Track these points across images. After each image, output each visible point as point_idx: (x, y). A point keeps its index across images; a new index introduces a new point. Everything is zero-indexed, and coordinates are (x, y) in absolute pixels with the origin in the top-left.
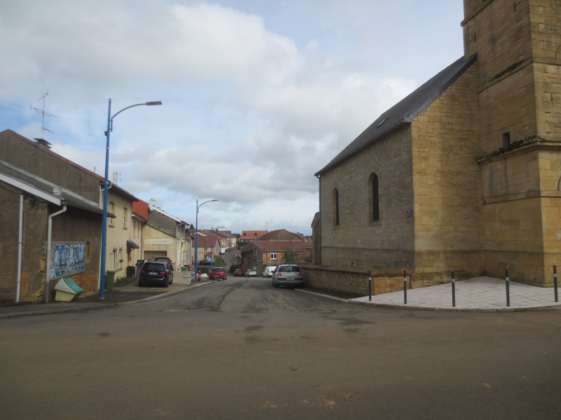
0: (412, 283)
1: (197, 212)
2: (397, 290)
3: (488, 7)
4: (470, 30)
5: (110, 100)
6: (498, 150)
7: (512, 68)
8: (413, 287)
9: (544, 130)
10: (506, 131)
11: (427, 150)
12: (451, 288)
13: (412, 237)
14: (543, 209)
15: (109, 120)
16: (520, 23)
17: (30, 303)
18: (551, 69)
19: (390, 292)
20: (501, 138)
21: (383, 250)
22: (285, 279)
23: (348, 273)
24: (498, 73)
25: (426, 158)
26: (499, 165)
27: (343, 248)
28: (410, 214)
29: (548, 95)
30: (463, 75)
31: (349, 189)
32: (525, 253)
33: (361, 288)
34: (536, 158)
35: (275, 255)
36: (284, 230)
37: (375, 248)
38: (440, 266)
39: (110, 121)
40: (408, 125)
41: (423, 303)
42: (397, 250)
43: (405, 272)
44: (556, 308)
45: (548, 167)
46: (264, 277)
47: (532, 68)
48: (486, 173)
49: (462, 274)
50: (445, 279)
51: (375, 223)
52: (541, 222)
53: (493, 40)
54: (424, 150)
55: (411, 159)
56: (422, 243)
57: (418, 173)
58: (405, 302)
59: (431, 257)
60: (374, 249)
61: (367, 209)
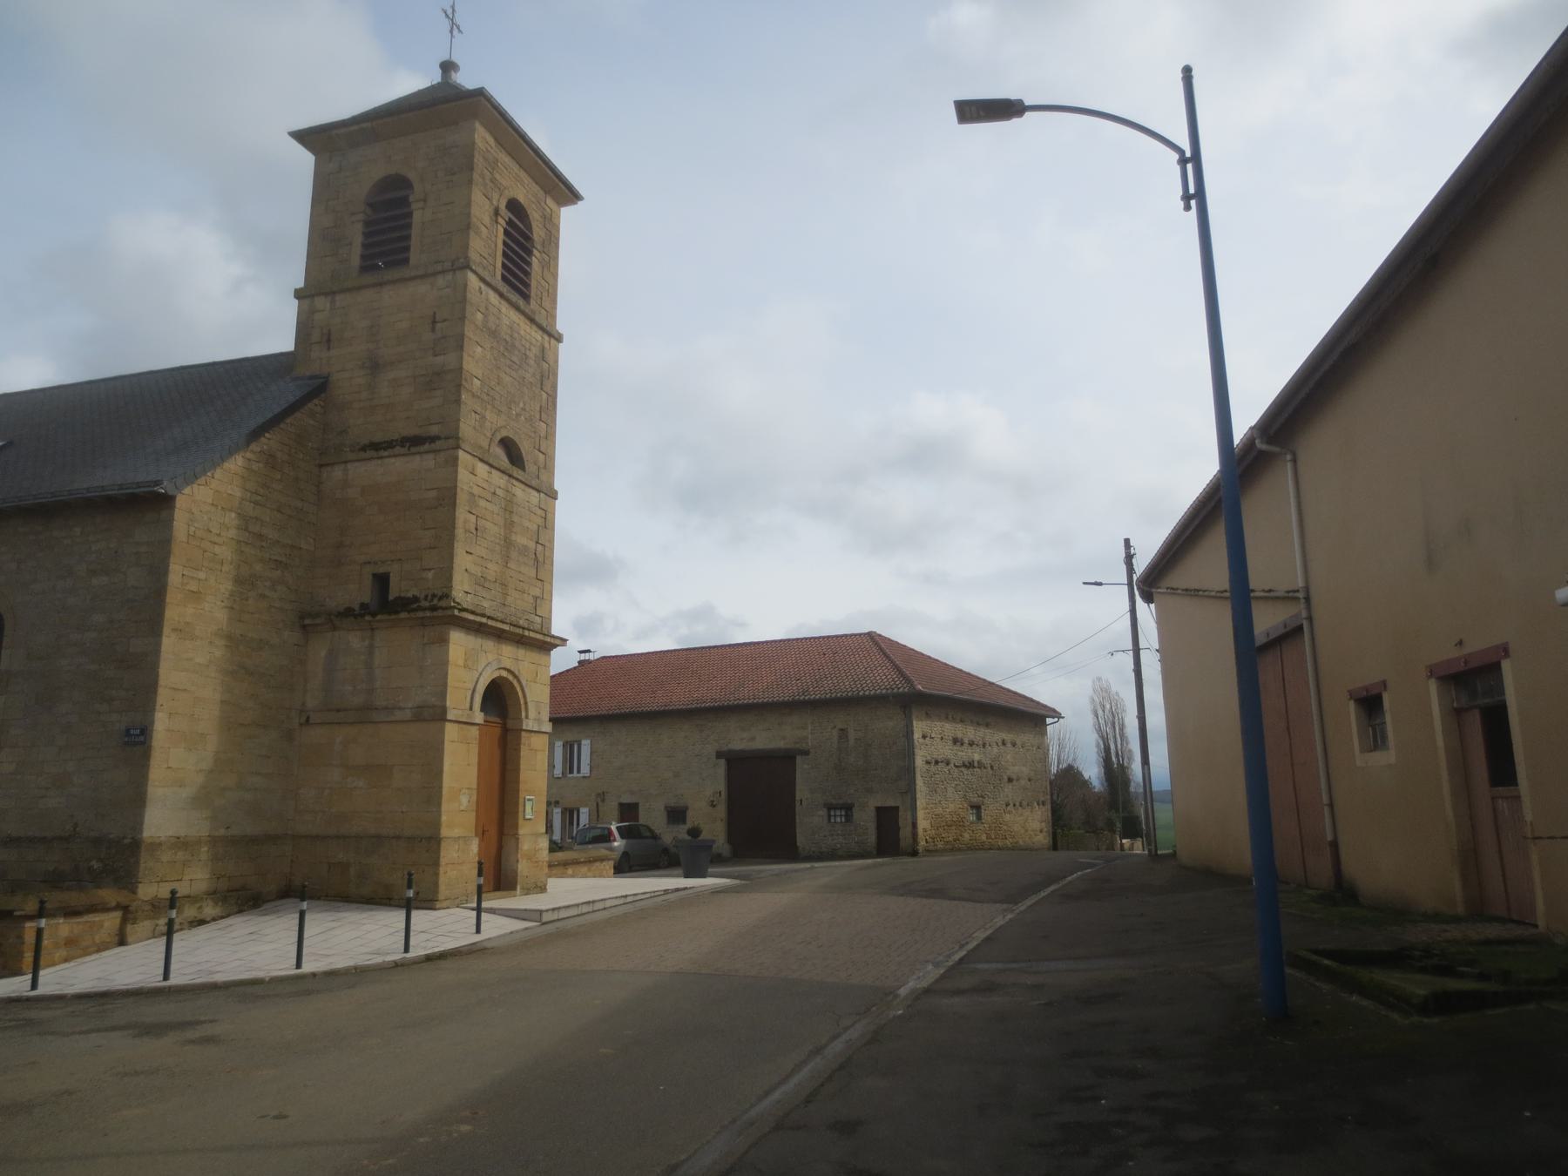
7: (414, 442)
8: (130, 939)
10: (381, 570)
11: (202, 575)
12: (297, 921)
13: (137, 799)
14: (448, 748)
16: (440, 359)
17: (959, 850)
19: (66, 960)
20: (368, 581)
25: (196, 596)
26: (355, 640)
29: (473, 518)
30: (298, 415)
32: (398, 838)
34: (444, 641)
38: (196, 878)
40: (167, 501)
41: (212, 973)
44: (488, 945)
45: (461, 662)
47: (456, 459)
48: (319, 651)
49: (243, 898)
50: (209, 910)
52: (441, 772)
57: (175, 630)
59: (181, 855)
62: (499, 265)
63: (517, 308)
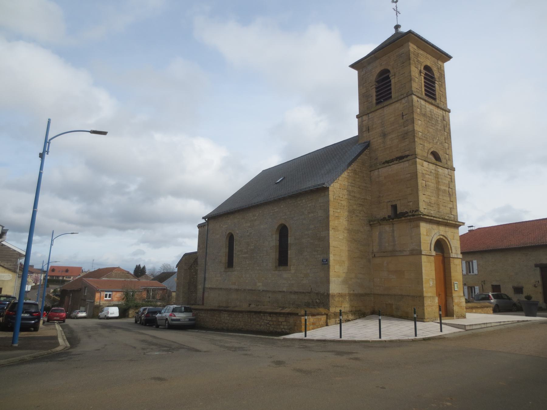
0: (328, 321)
1: (52, 245)
2: (318, 328)
3: (380, 110)
4: (364, 122)
5: (49, 120)
6: (387, 217)
7: (400, 158)
8: (329, 324)
9: (423, 208)
10: (394, 204)
11: (339, 211)
13: (327, 281)
14: (423, 264)
15: (46, 142)
16: (406, 128)
18: (425, 164)
19: (313, 329)
20: (390, 208)
21: (291, 292)
22: (178, 320)
23: (265, 313)
24: (388, 159)
25: (338, 217)
26: (387, 228)
27: (237, 290)
28: (326, 263)
29: (424, 182)
31: (249, 236)
32: (408, 296)
33: (282, 327)
34: (418, 226)
35: (110, 295)
36: (118, 269)
37: (281, 290)
38: (346, 306)
39: (47, 142)
40: (327, 189)
42: (309, 293)
43: (340, 311)
44: (446, 337)
45: (425, 234)
46: (101, 319)
51: (282, 268)
53: (384, 135)
54: (337, 211)
55: (328, 217)
56: (336, 287)
58: (341, 337)
60: (280, 292)
61: (274, 255)
62: (423, 90)
63: (432, 104)
